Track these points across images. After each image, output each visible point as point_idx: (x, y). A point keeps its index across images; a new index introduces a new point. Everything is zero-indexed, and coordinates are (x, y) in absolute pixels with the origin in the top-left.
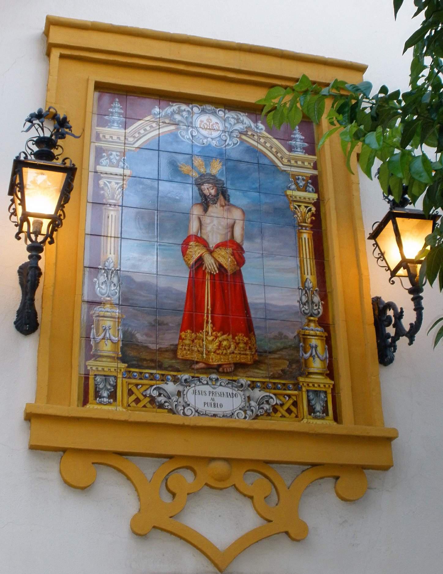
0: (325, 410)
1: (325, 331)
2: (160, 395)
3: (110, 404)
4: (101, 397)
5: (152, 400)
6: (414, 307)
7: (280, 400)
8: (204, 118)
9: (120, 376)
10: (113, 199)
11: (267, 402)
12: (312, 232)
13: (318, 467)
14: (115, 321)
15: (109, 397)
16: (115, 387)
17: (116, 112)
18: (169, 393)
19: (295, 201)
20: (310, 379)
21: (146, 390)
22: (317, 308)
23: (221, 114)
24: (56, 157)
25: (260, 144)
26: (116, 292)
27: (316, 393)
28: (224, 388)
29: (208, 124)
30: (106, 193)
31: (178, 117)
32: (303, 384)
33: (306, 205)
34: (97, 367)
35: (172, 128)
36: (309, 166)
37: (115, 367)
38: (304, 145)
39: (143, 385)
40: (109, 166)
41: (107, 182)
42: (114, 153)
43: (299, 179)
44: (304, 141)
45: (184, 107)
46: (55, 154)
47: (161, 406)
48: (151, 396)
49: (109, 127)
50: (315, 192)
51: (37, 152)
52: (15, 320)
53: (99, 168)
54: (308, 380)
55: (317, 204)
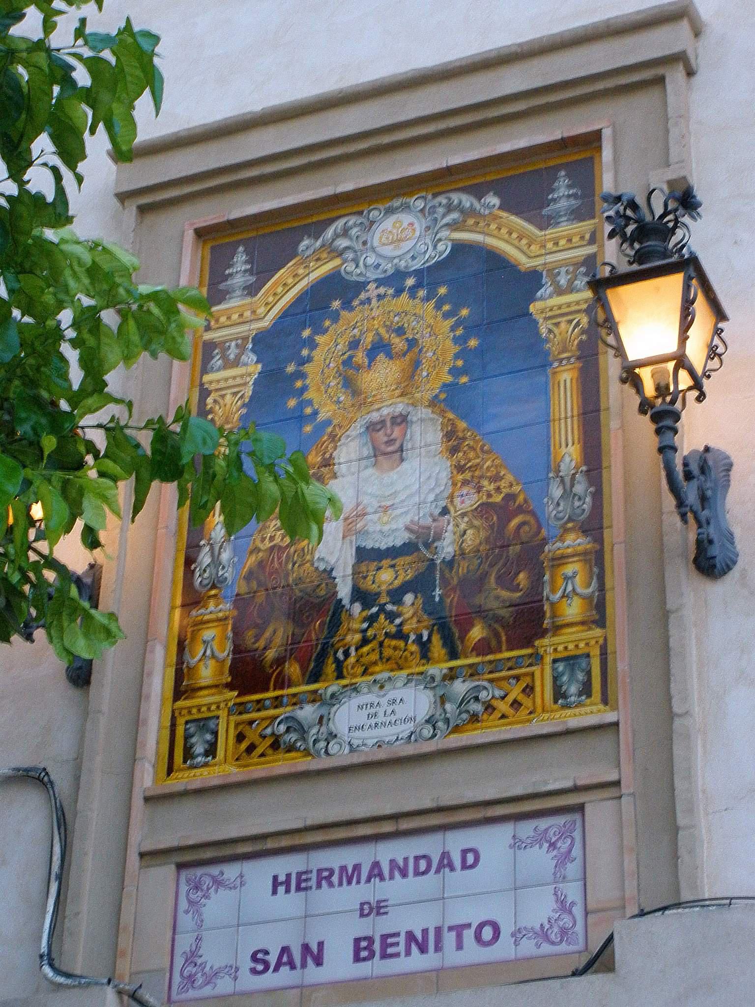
0: (586, 690)
2: (288, 730)
8: (389, 223)
11: (477, 699)
20: (199, 700)
26: (584, 510)
27: (571, 660)
31: (343, 243)
32: (545, 651)
35: (337, 262)
42: (563, 270)
47: (291, 748)
54: (556, 639)
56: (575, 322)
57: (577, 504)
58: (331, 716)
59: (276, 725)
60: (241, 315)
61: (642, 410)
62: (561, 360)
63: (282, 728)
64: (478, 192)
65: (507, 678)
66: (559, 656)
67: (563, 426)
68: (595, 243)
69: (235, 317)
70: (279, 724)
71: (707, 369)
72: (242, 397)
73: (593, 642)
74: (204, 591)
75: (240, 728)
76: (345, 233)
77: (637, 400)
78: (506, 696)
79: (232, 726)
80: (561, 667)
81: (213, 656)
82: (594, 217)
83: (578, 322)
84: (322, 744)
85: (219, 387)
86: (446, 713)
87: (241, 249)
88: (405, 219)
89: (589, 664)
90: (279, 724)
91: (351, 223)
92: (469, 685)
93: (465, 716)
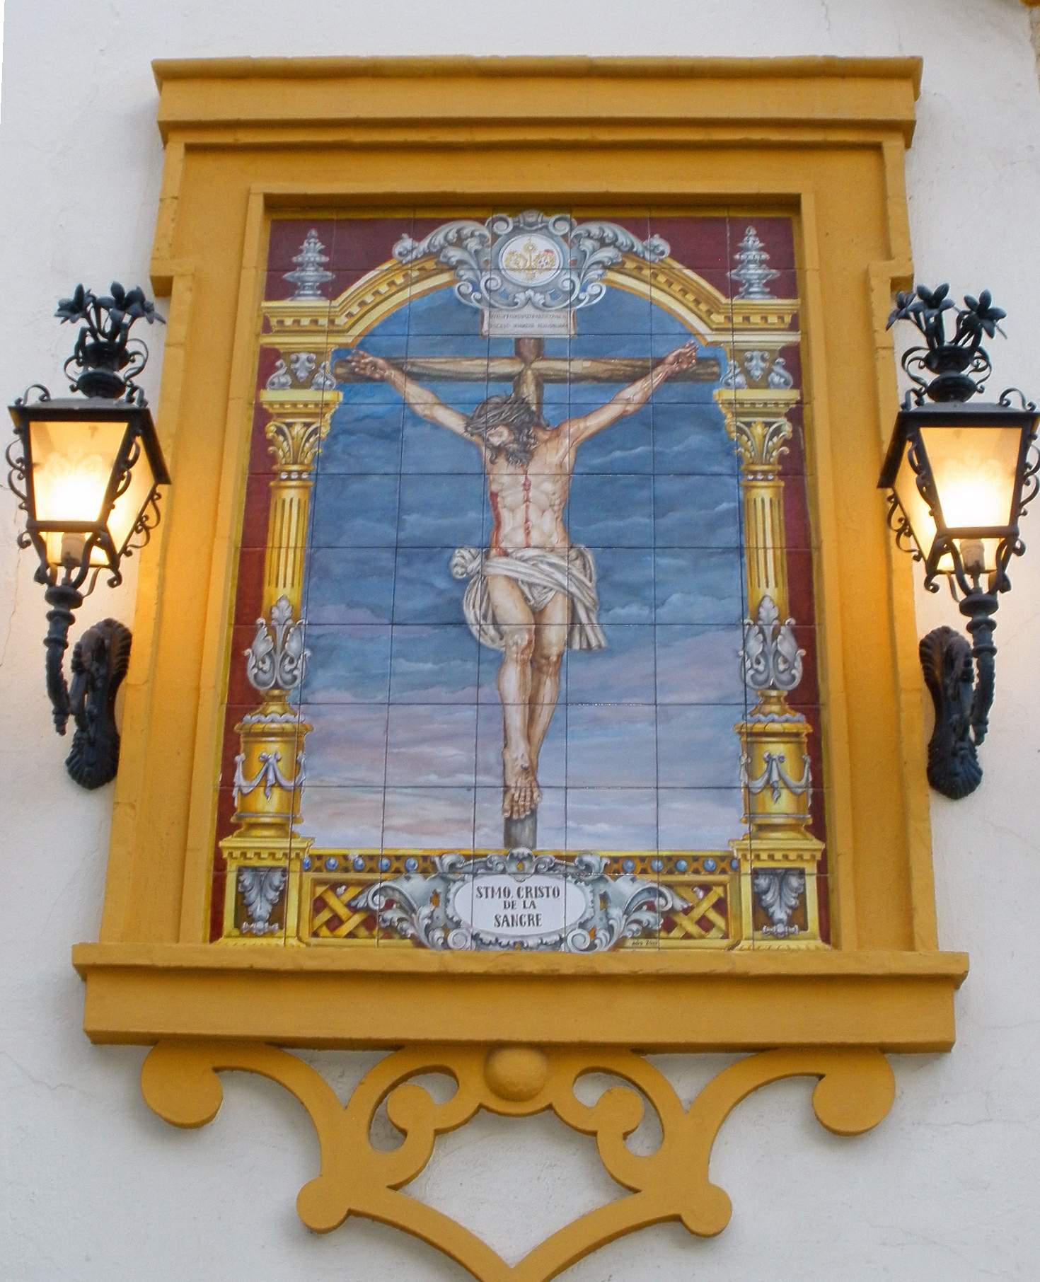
0: (797, 917)
1: (809, 721)
2: (389, 905)
6: (46, 635)
7: (683, 899)
8: (519, 244)
9: (296, 866)
12: (782, 484)
13: (650, 1057)
14: (800, 743)
15: (790, 923)
16: (283, 894)
18: (408, 896)
19: (280, 415)
23: (563, 228)
24: (979, 386)
26: (295, 678)
27: (781, 876)
28: (545, 878)
29: (527, 257)
30: (280, 451)
31: (455, 255)
32: (231, 854)
34: (801, 853)
35: (444, 278)
39: (348, 884)
40: (293, 386)
41: (742, 425)
44: (770, 264)
45: (469, 227)
46: (123, 379)
47: (391, 931)
48: (367, 909)
50: (794, 387)
51: (933, 384)
52: (68, 755)
55: (797, 414)
60: (297, 322)
61: (41, 577)
63: (380, 901)
64: (639, 230)
65: (689, 885)
66: (248, 863)
68: (798, 331)
70: (374, 895)
71: (129, 544)
73: (807, 856)
74: (262, 689)
75: (320, 890)
77: (37, 563)
79: (307, 887)
80: (763, 882)
81: (278, 784)
82: (795, 297)
84: (438, 934)
85: (282, 411)
86: (608, 919)
88: (541, 243)
89: (286, 883)
90: (374, 895)
91: (466, 232)
93: (635, 927)
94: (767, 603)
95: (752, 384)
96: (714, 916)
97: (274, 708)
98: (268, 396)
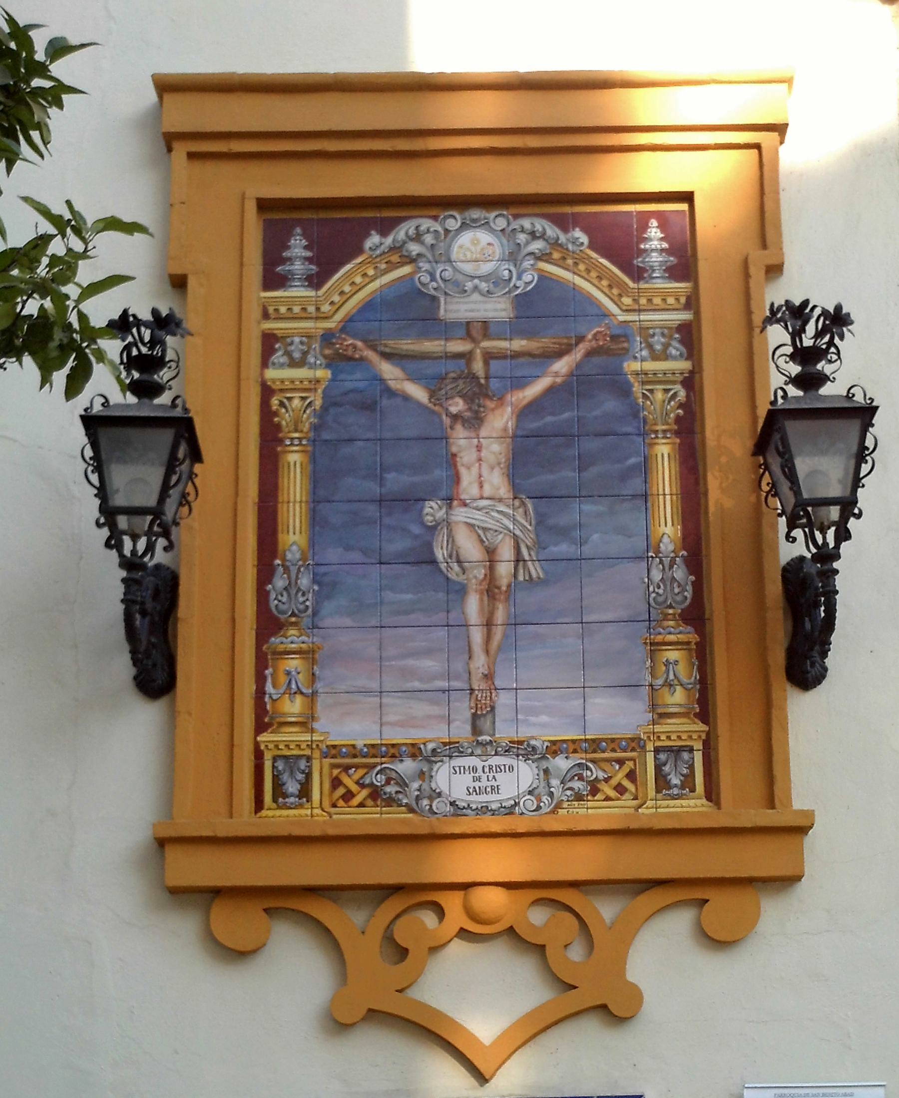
0: (688, 782)
2: (388, 782)
3: (301, 806)
4: (285, 796)
5: (375, 794)
7: (604, 771)
10: (296, 431)
12: (678, 441)
17: (652, 250)
21: (362, 778)
22: (305, 598)
23: (501, 223)
25: (579, 275)
26: (307, 606)
27: (676, 752)
29: (473, 249)
33: (304, 395)
34: (690, 734)
35: (406, 270)
36: (678, 306)
37: (307, 741)
38: (670, 261)
39: (357, 767)
41: (645, 392)
43: (653, 336)
45: (426, 224)
47: (390, 801)
49: (647, 282)
53: (271, 374)
55: (691, 382)
56: (672, 392)
57: (301, 599)
58: (433, 774)
59: (374, 775)
62: (292, 439)
63: (381, 778)
67: (291, 509)
69: (297, 309)
70: (377, 774)
71: (767, 473)
72: (310, 404)
75: (336, 772)
76: (418, 238)
78: (610, 777)
80: (662, 757)
83: (675, 393)
84: (425, 802)
87: (298, 230)
88: (484, 237)
89: (310, 767)
92: (569, 764)
93: (569, 793)
94: (666, 540)
95: (655, 357)
96: (626, 783)
97: (292, 632)
98: (271, 374)
